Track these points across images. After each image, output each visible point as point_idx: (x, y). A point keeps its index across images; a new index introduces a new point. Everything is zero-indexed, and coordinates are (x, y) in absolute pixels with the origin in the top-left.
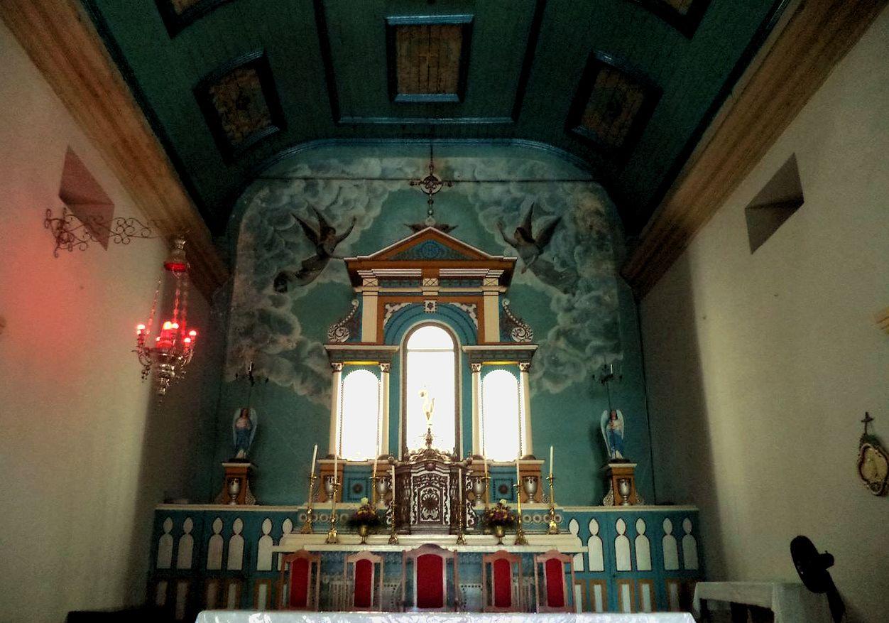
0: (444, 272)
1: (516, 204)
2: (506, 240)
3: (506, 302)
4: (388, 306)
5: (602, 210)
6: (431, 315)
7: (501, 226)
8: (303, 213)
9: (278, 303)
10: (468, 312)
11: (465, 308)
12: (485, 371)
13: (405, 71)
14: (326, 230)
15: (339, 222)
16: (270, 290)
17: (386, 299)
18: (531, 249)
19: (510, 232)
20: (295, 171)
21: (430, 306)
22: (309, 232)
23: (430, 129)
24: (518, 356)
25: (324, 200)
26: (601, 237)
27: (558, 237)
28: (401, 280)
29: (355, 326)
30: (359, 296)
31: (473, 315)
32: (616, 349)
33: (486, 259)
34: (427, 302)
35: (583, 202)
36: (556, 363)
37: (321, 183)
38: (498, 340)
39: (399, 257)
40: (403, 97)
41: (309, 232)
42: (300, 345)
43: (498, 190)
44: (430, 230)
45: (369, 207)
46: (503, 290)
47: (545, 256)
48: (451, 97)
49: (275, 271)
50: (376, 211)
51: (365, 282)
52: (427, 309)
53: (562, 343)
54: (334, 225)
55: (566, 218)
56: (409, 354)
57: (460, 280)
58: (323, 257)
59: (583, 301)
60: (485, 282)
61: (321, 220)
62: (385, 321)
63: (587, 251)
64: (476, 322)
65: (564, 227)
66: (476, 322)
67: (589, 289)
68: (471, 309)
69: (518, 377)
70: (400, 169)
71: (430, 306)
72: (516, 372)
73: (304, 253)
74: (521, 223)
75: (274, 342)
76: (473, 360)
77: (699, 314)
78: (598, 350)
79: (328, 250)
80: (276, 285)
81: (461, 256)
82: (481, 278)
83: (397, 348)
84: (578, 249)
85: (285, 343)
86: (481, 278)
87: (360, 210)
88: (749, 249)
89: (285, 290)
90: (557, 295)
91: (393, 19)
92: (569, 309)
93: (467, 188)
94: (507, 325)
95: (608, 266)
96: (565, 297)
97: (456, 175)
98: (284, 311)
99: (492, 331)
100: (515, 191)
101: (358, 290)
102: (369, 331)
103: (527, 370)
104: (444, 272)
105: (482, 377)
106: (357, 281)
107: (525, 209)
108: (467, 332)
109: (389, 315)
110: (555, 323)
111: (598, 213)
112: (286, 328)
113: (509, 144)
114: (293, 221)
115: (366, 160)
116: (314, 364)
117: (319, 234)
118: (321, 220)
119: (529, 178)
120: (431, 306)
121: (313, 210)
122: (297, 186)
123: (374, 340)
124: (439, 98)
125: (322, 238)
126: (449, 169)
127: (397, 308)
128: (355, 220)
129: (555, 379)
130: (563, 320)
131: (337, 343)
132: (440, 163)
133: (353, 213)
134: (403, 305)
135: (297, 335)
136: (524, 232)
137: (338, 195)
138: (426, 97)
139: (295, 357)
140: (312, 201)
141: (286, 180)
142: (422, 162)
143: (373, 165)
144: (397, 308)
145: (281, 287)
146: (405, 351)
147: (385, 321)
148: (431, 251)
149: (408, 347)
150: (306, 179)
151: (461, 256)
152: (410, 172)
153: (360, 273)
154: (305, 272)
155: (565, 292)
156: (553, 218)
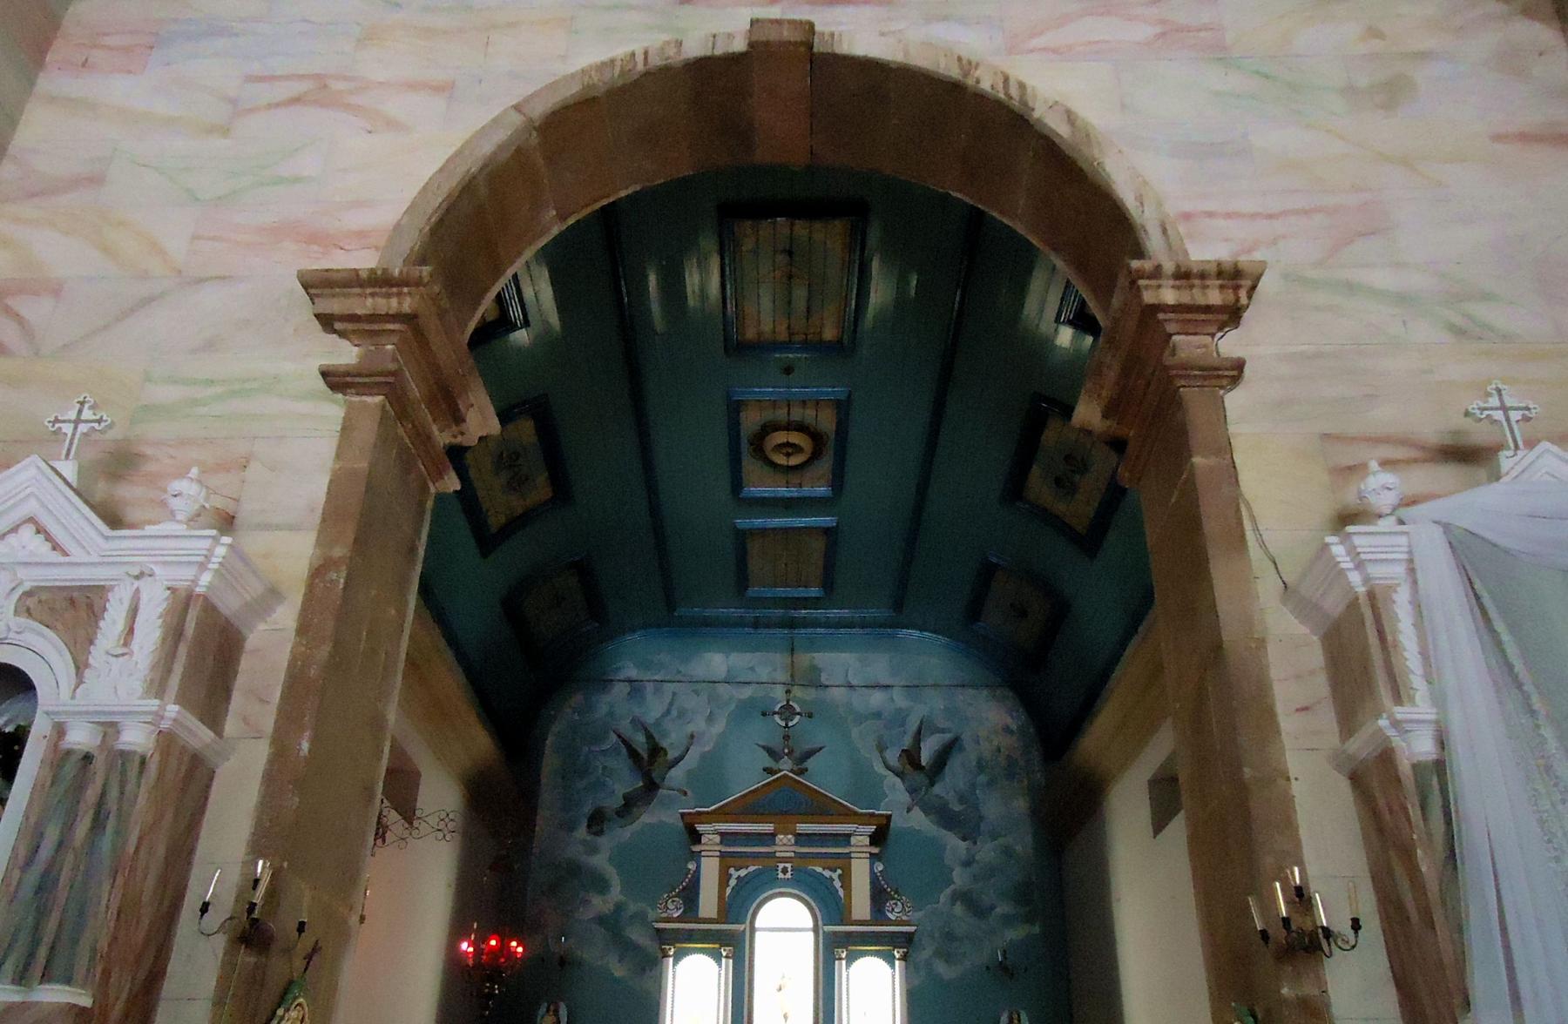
0: (803, 828)
1: (900, 718)
2: (888, 767)
3: (880, 867)
4: (732, 871)
5: (1014, 727)
6: (786, 883)
7: (882, 749)
8: (625, 727)
9: (594, 850)
10: (832, 879)
11: (827, 873)
12: (851, 959)
13: (755, 565)
14: (656, 750)
15: (672, 741)
16: (581, 832)
17: (730, 861)
18: (920, 778)
19: (893, 756)
20: (618, 669)
21: (785, 871)
22: (633, 754)
23: (785, 623)
24: (894, 940)
25: (653, 710)
26: (1011, 762)
27: (955, 764)
28: (749, 838)
29: (690, 895)
30: (696, 857)
31: (837, 884)
32: (1029, 919)
33: (856, 813)
34: (781, 866)
35: (990, 720)
36: (950, 937)
37: (650, 687)
38: (868, 917)
39: (748, 808)
40: (753, 591)
41: (633, 754)
42: (619, 908)
43: (877, 699)
44: (785, 776)
45: (710, 719)
46: (875, 850)
47: (938, 789)
48: (814, 592)
49: (587, 809)
50: (719, 727)
51: (704, 840)
52: (781, 875)
53: (958, 909)
54: (664, 744)
55: (966, 738)
56: (758, 934)
57: (823, 839)
58: (652, 787)
59: (987, 852)
60: (853, 840)
61: (649, 737)
62: (728, 891)
63: (991, 783)
64: (841, 892)
65: (962, 749)
66: (841, 892)
67: (994, 836)
68: (835, 876)
69: (893, 966)
70: (752, 669)
71: (785, 871)
72: (890, 960)
73: (624, 781)
74: (907, 742)
75: (586, 902)
76: (837, 944)
77: (1114, 896)
78: (1008, 920)
79: (657, 781)
80: (589, 826)
81: (823, 808)
82: (849, 836)
83: (741, 927)
84: (983, 778)
85: (600, 904)
86: (849, 836)
87: (698, 725)
88: (1150, 828)
89: (600, 833)
90: (955, 844)
91: (742, 523)
92: (967, 864)
93: (838, 694)
94: (879, 896)
95: (1021, 805)
96: (963, 845)
97: (824, 679)
98: (600, 861)
99: (861, 905)
100: (900, 699)
101: (696, 848)
102: (708, 903)
103: (904, 958)
104: (803, 828)
105: (848, 966)
106: (696, 837)
107: (913, 725)
108: (829, 906)
109: (733, 882)
110: (950, 882)
111: (1007, 730)
112: (601, 885)
113: (893, 636)
114: (614, 737)
115: (708, 655)
116: (637, 935)
117: (645, 756)
118: (649, 737)
119: (916, 682)
120: (785, 871)
121: (638, 723)
122: (620, 690)
123: (714, 915)
124: (800, 592)
125: (649, 762)
126: (815, 669)
127: (743, 873)
128: (692, 736)
129: (948, 958)
130: (960, 878)
131: (669, 920)
132: (804, 659)
133: (691, 728)
134: (752, 868)
135: (616, 893)
136: (911, 757)
137: (671, 704)
138: (781, 591)
139: (612, 924)
140: (637, 711)
141: (605, 683)
142: (780, 658)
143: (716, 662)
144: (743, 873)
145: (595, 829)
146: (753, 930)
147: (728, 891)
148: (786, 800)
149: (758, 924)
150: (630, 681)
151: (823, 808)
152: (764, 674)
153: (700, 828)
154: (629, 806)
155: (964, 839)
156: (948, 736)
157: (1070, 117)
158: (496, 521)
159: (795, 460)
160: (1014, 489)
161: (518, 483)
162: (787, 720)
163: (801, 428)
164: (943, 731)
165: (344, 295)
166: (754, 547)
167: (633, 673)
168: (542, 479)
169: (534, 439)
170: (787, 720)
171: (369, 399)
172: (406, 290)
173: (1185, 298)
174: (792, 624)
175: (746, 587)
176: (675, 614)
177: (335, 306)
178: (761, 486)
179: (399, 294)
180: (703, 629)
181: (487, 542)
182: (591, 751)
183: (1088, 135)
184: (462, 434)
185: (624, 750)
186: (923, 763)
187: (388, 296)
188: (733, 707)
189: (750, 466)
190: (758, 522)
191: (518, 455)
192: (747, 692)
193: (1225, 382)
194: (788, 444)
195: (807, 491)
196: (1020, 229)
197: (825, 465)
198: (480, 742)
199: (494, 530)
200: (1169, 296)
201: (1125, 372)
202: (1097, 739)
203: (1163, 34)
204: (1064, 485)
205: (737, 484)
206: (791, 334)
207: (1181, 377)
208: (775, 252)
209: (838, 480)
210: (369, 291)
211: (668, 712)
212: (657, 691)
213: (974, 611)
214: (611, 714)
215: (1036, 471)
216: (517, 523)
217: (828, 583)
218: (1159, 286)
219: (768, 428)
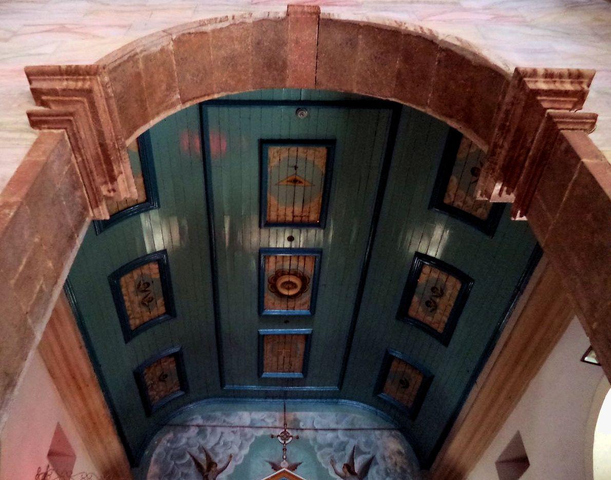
1: (342, 446)
2: (337, 473)
5: (403, 451)
7: (333, 462)
8: (195, 450)
13: (269, 358)
14: (211, 464)
15: (220, 458)
19: (339, 467)
20: (193, 419)
22: (198, 465)
23: (284, 394)
37: (209, 430)
41: (198, 465)
43: (330, 435)
44: (284, 472)
45: (241, 447)
48: (298, 375)
50: (245, 451)
54: (216, 460)
55: (378, 457)
61: (208, 456)
65: (377, 464)
70: (263, 420)
74: (346, 460)
87: (235, 449)
91: (262, 331)
93: (308, 434)
97: (301, 425)
107: (349, 450)
111: (400, 453)
114: (188, 457)
115: (240, 413)
117: (205, 467)
118: (208, 456)
119: (350, 427)
121: (202, 449)
122: (193, 431)
126: (296, 420)
128: (231, 456)
133: (230, 452)
138: (280, 375)
140: (202, 442)
141: (185, 426)
142: (278, 415)
143: (245, 416)
150: (198, 426)
152: (270, 422)
156: (368, 456)
157: (458, 39)
158: (134, 323)
159: (292, 293)
160: (403, 313)
161: (147, 303)
162: (285, 440)
163: (296, 274)
164: (365, 453)
165: (50, 80)
166: (268, 348)
167: (200, 421)
168: (160, 301)
169: (158, 276)
170: (285, 440)
171: (55, 131)
172: (88, 77)
173: (552, 87)
174: (285, 396)
175: (262, 372)
176: (226, 392)
177: (44, 85)
178: (275, 309)
179: (84, 80)
180: (239, 398)
181: (129, 334)
182: (175, 464)
183: (468, 43)
184: (114, 190)
185: (193, 463)
186: (356, 471)
187: (77, 80)
188: (253, 440)
189: (269, 298)
190: (270, 331)
191: (148, 284)
192: (261, 433)
193: (587, 127)
194: (289, 282)
195: (297, 312)
196: (429, 111)
197: (306, 297)
198: (115, 447)
199: (133, 328)
200: (542, 85)
201: (513, 148)
202: (456, 447)
203: (494, 18)
204: (431, 305)
205: (261, 307)
206: (294, 216)
207: (561, 123)
208: (288, 166)
209: (313, 308)
210: (65, 77)
211: (218, 443)
212: (213, 432)
213: (380, 387)
214: (187, 444)
215: (416, 299)
216: (145, 327)
217: (305, 370)
218: (536, 81)
219: (280, 273)
